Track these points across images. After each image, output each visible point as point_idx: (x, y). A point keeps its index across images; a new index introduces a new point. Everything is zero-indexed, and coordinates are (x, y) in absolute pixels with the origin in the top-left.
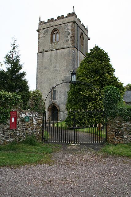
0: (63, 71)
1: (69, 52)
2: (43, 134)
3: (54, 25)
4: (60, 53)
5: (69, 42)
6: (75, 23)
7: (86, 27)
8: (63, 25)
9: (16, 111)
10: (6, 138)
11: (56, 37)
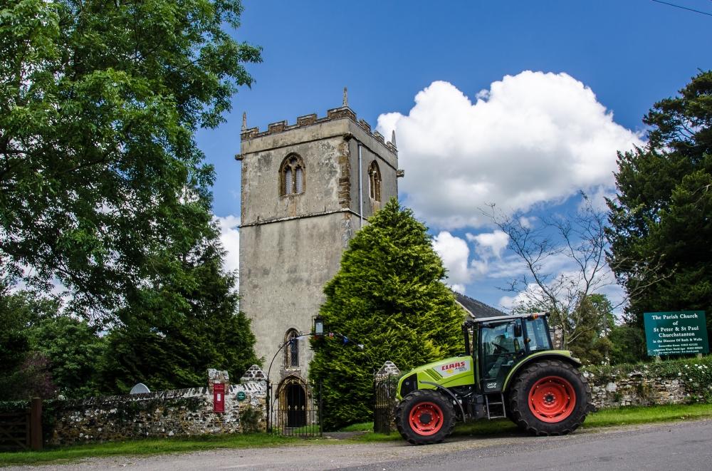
0: (318, 281)
1: (334, 227)
2: (268, 423)
3: (289, 143)
4: (307, 229)
5: (335, 197)
6: (352, 140)
7: (388, 139)
8: (316, 142)
9: (224, 384)
10: (208, 426)
11: (295, 180)
